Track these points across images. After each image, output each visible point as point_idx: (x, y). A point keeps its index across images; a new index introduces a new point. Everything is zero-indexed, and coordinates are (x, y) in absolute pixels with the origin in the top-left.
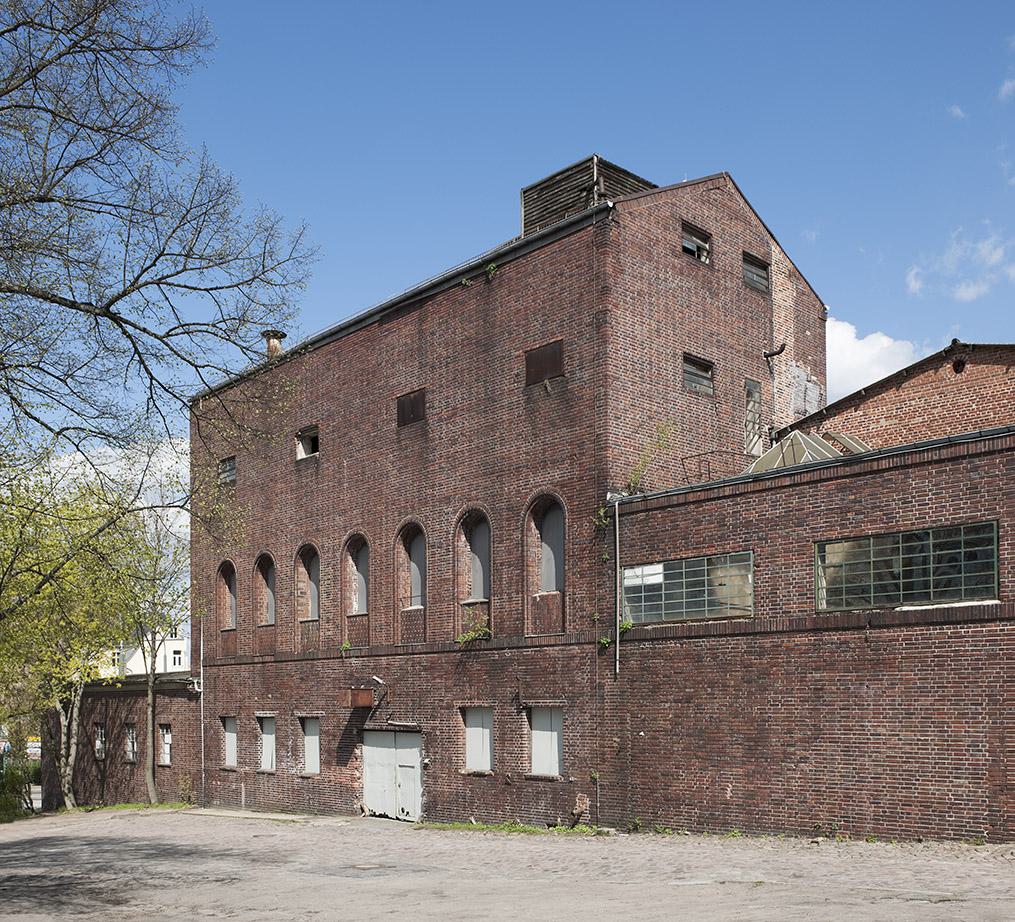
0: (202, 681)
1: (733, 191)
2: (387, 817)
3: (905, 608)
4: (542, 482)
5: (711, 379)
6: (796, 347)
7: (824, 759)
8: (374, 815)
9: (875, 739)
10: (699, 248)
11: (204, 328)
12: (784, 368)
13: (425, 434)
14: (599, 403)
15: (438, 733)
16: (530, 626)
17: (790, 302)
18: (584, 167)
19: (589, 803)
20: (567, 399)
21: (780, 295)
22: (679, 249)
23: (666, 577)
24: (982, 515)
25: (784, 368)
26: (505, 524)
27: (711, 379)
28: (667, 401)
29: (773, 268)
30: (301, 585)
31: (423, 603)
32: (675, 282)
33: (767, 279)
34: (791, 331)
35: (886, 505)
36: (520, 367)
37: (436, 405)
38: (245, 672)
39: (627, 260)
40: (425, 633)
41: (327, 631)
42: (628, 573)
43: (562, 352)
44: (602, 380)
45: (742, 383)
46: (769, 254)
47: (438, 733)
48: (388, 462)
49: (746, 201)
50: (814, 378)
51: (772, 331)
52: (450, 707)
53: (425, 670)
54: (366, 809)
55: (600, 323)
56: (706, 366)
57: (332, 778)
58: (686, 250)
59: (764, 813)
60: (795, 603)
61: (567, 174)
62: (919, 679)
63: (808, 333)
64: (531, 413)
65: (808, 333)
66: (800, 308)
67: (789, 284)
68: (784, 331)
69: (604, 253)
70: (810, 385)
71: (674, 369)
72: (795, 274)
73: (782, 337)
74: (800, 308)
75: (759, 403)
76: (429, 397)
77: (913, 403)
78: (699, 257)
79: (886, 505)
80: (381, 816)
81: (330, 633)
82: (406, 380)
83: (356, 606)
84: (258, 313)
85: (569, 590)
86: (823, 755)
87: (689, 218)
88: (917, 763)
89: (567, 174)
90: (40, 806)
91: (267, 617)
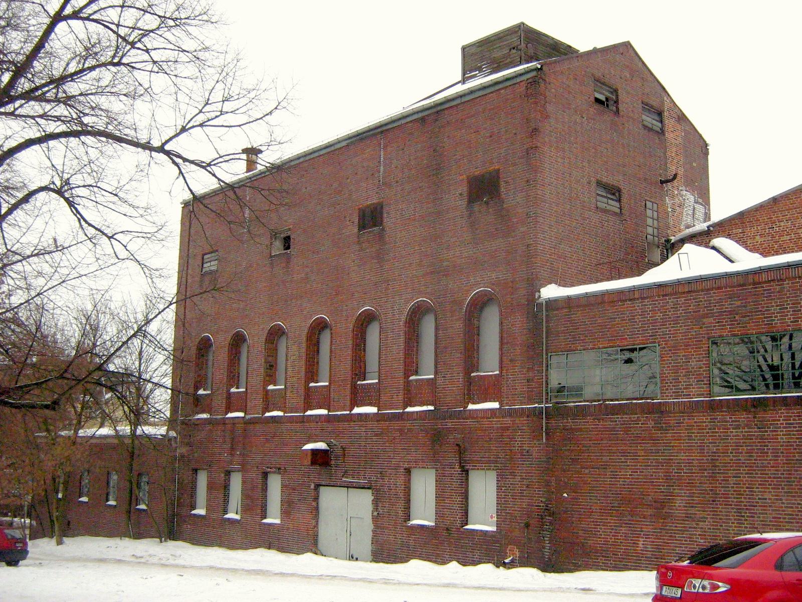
6: (686, 176)
7: (720, 519)
9: (762, 503)
10: (607, 99)
11: (237, 156)
12: (676, 192)
19: (518, 554)
21: (672, 135)
22: (592, 99)
25: (676, 192)
35: (766, 310)
36: (464, 189)
46: (663, 102)
50: (700, 200)
52: (397, 468)
53: (376, 435)
58: (597, 100)
59: (737, 351)
60: (693, 388)
62: (798, 453)
67: (679, 127)
70: (697, 206)
73: (674, 168)
77: (782, 224)
79: (766, 310)
84: (755, 345)
86: (718, 515)
87: (598, 74)
88: (798, 523)
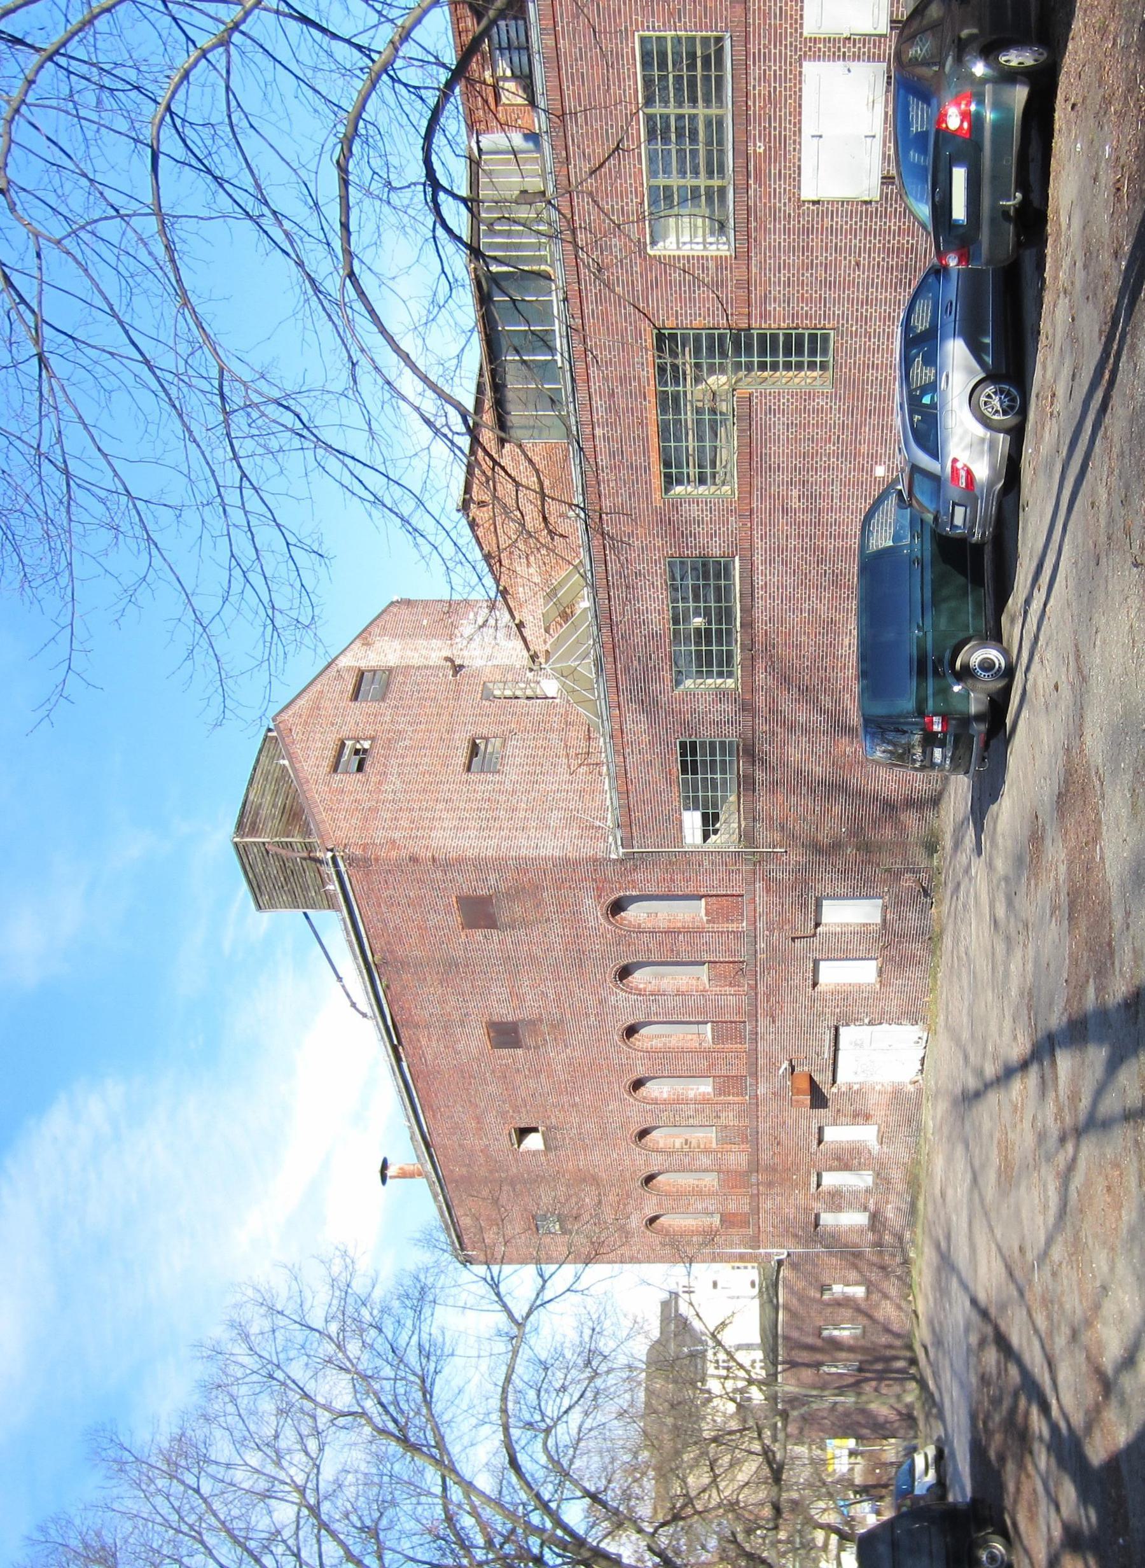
0: (775, 1250)
1: (290, 712)
2: (923, 1058)
3: (738, 624)
4: (593, 911)
5: (487, 739)
8: (922, 1071)
13: (532, 1023)
14: (523, 865)
15: (838, 1010)
16: (735, 925)
17: (397, 644)
18: (241, 851)
20: (516, 893)
23: (696, 808)
24: (662, 568)
26: (632, 948)
27: (487, 739)
28: (514, 792)
29: (363, 664)
30: (678, 1145)
31: (706, 1023)
32: (394, 783)
33: (375, 671)
34: (425, 643)
36: (479, 934)
37: (505, 1013)
38: (767, 1205)
39: (380, 836)
40: (735, 1022)
41: (729, 1118)
42: (689, 840)
43: (468, 898)
44: (498, 864)
45: (487, 703)
46: (349, 669)
47: (838, 1010)
48: (556, 1056)
49: (299, 696)
51: (426, 667)
54: (916, 1079)
55: (447, 864)
56: (474, 750)
57: (883, 1113)
58: (360, 768)
61: (247, 866)
63: (425, 623)
64: (526, 924)
65: (425, 623)
66: (399, 632)
67: (377, 645)
68: (433, 652)
69: (377, 860)
71: (482, 784)
72: (364, 636)
74: (399, 632)
75: (505, 683)
76: (495, 1018)
78: (365, 751)
80: (922, 1065)
81: (731, 1114)
82: (475, 1039)
83: (705, 1088)
85: (703, 891)
89: (247, 866)
90: (973, 70)
91: (710, 1181)
